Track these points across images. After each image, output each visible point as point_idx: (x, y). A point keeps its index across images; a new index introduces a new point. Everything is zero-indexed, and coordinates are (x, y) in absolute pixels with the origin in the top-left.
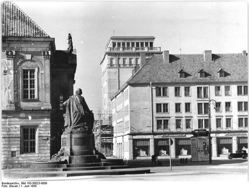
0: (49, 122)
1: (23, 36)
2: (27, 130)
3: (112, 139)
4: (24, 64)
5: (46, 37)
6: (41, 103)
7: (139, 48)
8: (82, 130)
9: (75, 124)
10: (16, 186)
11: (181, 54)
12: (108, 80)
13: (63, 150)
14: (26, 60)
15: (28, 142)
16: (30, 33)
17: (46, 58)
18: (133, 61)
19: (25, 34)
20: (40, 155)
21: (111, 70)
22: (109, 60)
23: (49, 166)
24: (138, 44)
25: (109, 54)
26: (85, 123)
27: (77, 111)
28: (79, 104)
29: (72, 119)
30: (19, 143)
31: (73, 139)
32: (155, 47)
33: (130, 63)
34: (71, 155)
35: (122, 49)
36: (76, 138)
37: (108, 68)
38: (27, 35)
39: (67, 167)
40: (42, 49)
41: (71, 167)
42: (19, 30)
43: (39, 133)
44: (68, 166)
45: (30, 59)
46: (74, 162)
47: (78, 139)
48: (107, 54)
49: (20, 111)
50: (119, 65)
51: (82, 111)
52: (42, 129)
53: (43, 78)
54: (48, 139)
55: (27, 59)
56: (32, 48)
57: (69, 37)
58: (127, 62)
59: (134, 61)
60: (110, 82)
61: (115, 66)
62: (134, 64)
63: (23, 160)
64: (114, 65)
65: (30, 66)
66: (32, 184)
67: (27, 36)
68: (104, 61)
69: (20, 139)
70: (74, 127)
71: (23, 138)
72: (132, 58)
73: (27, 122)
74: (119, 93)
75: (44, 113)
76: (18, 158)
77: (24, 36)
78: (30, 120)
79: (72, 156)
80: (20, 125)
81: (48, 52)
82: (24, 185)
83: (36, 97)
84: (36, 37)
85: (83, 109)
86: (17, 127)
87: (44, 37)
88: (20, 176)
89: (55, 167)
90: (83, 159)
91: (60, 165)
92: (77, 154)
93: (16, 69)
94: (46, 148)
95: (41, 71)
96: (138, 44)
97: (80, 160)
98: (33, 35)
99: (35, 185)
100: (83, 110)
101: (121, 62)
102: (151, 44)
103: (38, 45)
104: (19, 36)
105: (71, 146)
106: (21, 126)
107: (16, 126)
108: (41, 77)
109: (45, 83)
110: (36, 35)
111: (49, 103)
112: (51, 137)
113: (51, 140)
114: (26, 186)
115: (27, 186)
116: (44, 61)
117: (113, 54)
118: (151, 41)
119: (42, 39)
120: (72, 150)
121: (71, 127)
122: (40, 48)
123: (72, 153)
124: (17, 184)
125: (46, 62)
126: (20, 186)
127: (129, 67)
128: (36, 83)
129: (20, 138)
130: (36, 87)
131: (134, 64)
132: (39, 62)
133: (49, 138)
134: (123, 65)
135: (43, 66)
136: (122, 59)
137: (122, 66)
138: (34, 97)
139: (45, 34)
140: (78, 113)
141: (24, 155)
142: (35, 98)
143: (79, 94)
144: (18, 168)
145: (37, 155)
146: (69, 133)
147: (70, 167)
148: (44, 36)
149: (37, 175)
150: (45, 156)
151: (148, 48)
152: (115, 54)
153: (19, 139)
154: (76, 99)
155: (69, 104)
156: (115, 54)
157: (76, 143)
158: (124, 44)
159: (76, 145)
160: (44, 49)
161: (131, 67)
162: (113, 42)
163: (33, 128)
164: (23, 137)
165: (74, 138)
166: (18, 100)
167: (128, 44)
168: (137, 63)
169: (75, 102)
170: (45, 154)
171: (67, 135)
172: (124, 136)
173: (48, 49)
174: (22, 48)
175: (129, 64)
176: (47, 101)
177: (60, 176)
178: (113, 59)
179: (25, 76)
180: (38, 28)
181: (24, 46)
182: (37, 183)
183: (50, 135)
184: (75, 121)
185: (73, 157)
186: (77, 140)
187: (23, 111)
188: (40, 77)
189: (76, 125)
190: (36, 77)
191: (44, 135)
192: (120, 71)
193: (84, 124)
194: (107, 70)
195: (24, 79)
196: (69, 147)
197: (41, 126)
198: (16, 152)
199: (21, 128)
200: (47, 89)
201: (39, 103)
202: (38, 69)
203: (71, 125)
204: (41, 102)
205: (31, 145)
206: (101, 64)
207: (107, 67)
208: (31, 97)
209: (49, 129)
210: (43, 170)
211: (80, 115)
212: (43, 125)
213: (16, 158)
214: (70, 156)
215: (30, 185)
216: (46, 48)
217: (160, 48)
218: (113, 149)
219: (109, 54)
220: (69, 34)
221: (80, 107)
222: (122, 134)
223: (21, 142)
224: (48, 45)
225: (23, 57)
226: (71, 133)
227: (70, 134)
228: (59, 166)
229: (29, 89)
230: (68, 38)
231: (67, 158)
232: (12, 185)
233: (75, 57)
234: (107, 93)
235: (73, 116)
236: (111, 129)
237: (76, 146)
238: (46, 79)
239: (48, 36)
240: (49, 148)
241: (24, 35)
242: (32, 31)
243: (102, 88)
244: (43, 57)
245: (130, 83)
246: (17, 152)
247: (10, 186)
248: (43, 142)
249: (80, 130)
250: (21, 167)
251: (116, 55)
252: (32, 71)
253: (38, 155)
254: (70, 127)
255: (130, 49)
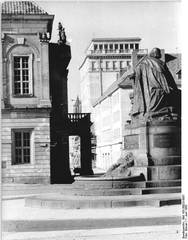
0: (48, 124)
1: (13, 13)
2: (20, 134)
3: (95, 148)
4: (15, 50)
5: (44, 14)
6: (37, 99)
7: (123, 51)
8: (168, 119)
9: (154, 110)
10: (186, 225)
11: (178, 53)
12: (90, 85)
13: (130, 156)
14: (18, 44)
15: (20, 150)
16: (22, 9)
17: (44, 41)
18: (117, 65)
19: (16, 11)
20: (37, 166)
21: (93, 74)
22: (90, 64)
23: (112, 186)
24: (121, 46)
25: (91, 57)
26: (171, 108)
27: (156, 85)
28: (158, 73)
29: (148, 100)
30: (10, 150)
31: (152, 137)
32: (141, 49)
33: (113, 67)
34: (149, 165)
35: (105, 52)
36: (158, 135)
37: (90, 72)
38: (18, 12)
39: (147, 187)
40: (37, 31)
41: (154, 187)
42: (8, 6)
43: (36, 139)
44: (148, 185)
45: (23, 44)
46: (157, 178)
47: (161, 136)
48: (88, 57)
49: (11, 110)
50: (102, 69)
51: (166, 87)
52: (39, 132)
53: (40, 68)
54: (47, 146)
55: (19, 44)
56: (25, 30)
57: (59, 26)
58: (110, 65)
59: (118, 64)
60: (92, 87)
61: (97, 70)
62: (119, 68)
63: (15, 172)
64: (95, 69)
65: (22, 52)
66: (185, 209)
67: (19, 13)
68: (83, 66)
69: (12, 145)
70: (151, 114)
71: (14, 145)
72: (116, 62)
73: (20, 124)
74: (106, 98)
75: (42, 113)
76: (9, 170)
77: (14, 13)
78: (23, 123)
79: (153, 167)
80: (10, 128)
81: (46, 35)
82: (185, 217)
83: (31, 92)
84: (30, 15)
85: (167, 82)
86: (7, 130)
87: (41, 15)
88: (63, 205)
89: (125, 188)
90: (173, 172)
91: (133, 183)
92: (160, 163)
93: (5, 56)
94: (44, 157)
95: (37, 59)
96: (121, 46)
97: (168, 173)
98: (26, 11)
99: (185, 206)
100: (167, 84)
101: (104, 65)
102: (137, 45)
103: (32, 25)
104: (9, 13)
105: (149, 149)
106: (12, 129)
107: (5, 129)
108: (36, 66)
109: (42, 73)
110: (29, 11)
111: (48, 100)
112: (51, 143)
113: (51, 147)
114: (186, 215)
115: (186, 214)
116: (41, 46)
117: (95, 57)
118: (137, 43)
119: (39, 17)
120: (151, 157)
121: (146, 114)
122: (36, 29)
123: (151, 162)
124: (184, 224)
125: (43, 47)
126: (186, 220)
127: (112, 71)
128: (30, 74)
129: (11, 145)
130: (31, 79)
131: (119, 68)
132: (34, 47)
133: (48, 144)
134: (106, 69)
135: (40, 52)
136: (104, 62)
137: (104, 70)
138: (28, 92)
139: (42, 10)
140: (159, 90)
141: (16, 167)
142: (30, 93)
143: (156, 57)
144: (9, 182)
145: (33, 167)
146: (143, 126)
147: (152, 187)
148: (40, 13)
149: (99, 203)
150: (44, 167)
151: (134, 50)
152: (97, 58)
153: (10, 146)
154: (153, 65)
155: (139, 74)
156: (97, 57)
157: (158, 144)
158: (106, 46)
159: (157, 147)
160: (39, 30)
161: (115, 71)
162: (94, 45)
163: (26, 132)
164: (15, 143)
165: (155, 135)
166: (8, 96)
167: (111, 46)
168: (122, 67)
169: (150, 70)
170: (44, 165)
171: (141, 128)
172: (112, 146)
173: (46, 30)
174: (12, 29)
175: (112, 67)
176: (45, 97)
177: (144, 205)
178: (95, 62)
179: (16, 65)
180: (31, 3)
181: (15, 27)
182: (183, 204)
183: (49, 141)
184: (152, 105)
185: (154, 169)
186: (160, 139)
187: (15, 110)
188: (35, 66)
189: (154, 111)
190: (30, 67)
191: (41, 141)
192: (102, 74)
193: (169, 110)
194: (89, 74)
195: (16, 69)
196: (146, 151)
197: (38, 129)
198: (7, 163)
199: (13, 132)
200: (44, 81)
201: (34, 98)
202: (33, 55)
203: (145, 112)
204: (36, 97)
205: (25, 154)
206: (79, 69)
207: (89, 71)
208: (24, 92)
209: (49, 133)
210: (104, 194)
211: (162, 94)
212: (41, 127)
213: (6, 170)
214: (148, 167)
215: (185, 211)
216: (42, 28)
217: (147, 49)
218: (96, 160)
219: (90, 57)
220: (60, 23)
221: (162, 79)
222: (110, 143)
223: (13, 149)
224: (46, 25)
225: (12, 41)
226: (148, 125)
227: (145, 128)
228: (132, 184)
229: (21, 81)
230: (58, 28)
231: (144, 171)
232: (185, 228)
233: (68, 48)
234: (89, 99)
235: (150, 96)
236: (94, 139)
237: (158, 148)
238: (43, 69)
239: (45, 13)
240: (49, 158)
241: (15, 12)
242: (24, 7)
243: (81, 95)
244: (40, 40)
245: (121, 86)
246: (8, 163)
247: (186, 230)
248: (41, 149)
249: (164, 120)
250: (13, 182)
251: (98, 57)
252: (26, 59)
253: (35, 167)
254: (144, 115)
255: (114, 51)
